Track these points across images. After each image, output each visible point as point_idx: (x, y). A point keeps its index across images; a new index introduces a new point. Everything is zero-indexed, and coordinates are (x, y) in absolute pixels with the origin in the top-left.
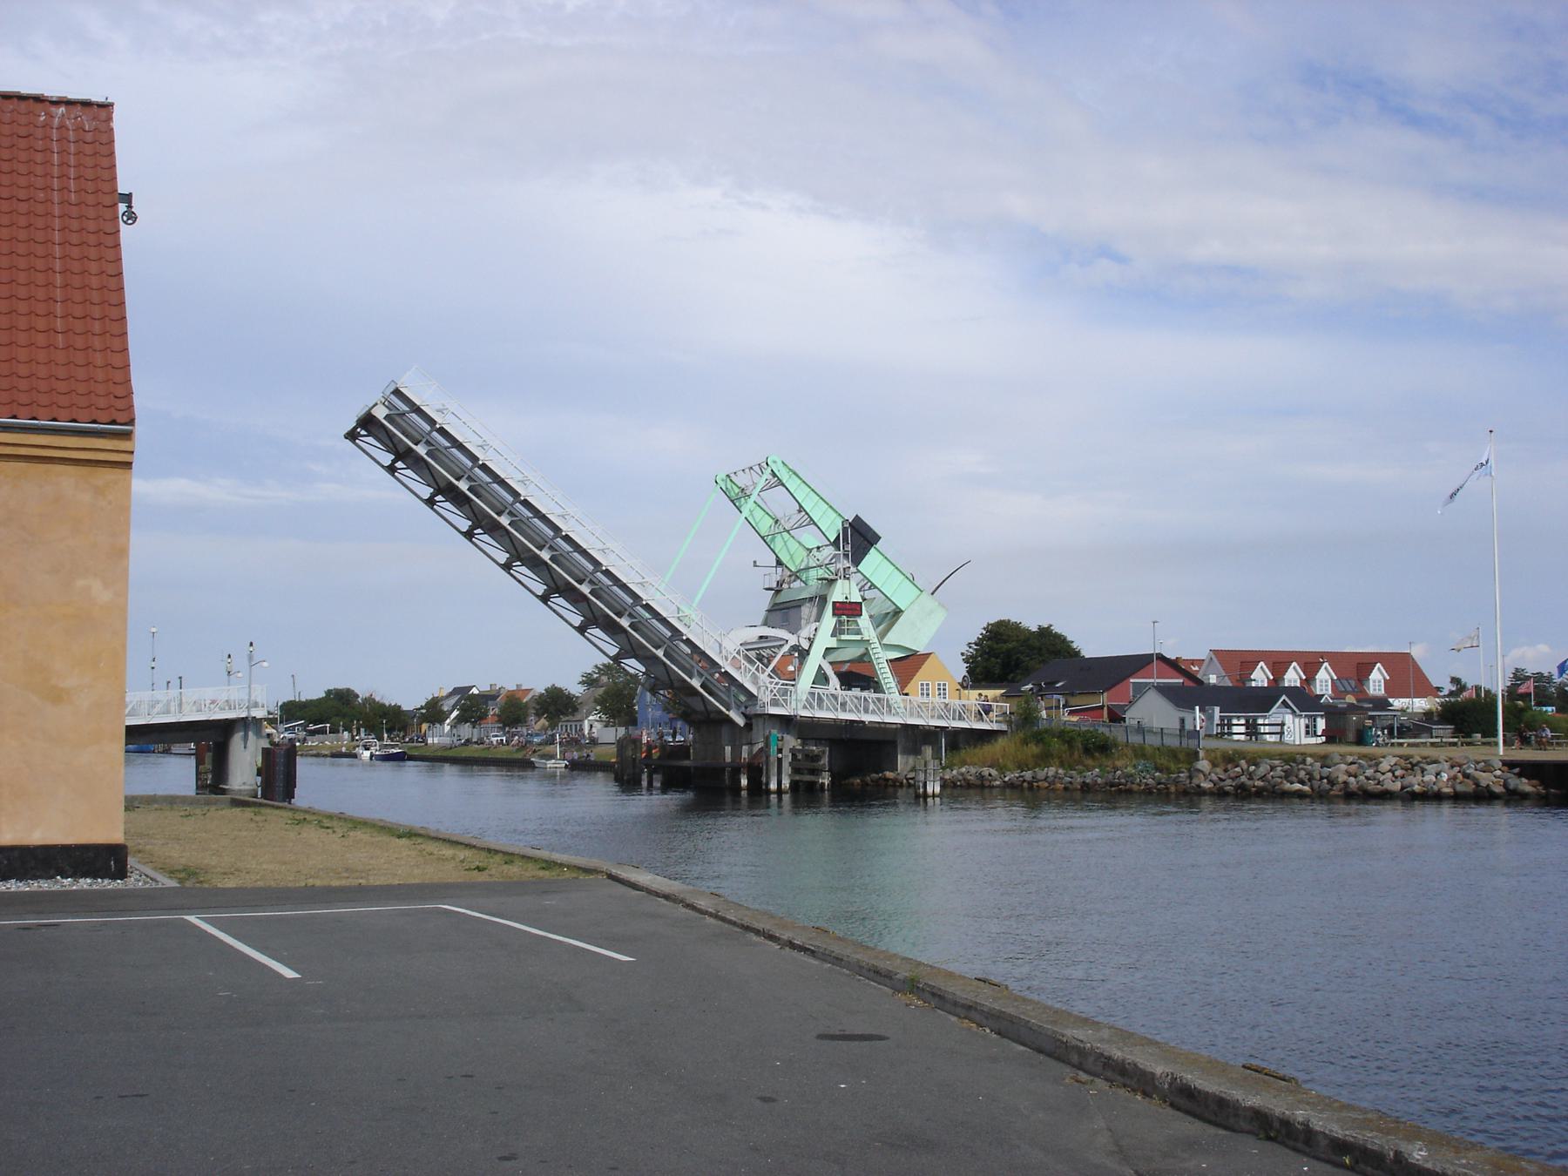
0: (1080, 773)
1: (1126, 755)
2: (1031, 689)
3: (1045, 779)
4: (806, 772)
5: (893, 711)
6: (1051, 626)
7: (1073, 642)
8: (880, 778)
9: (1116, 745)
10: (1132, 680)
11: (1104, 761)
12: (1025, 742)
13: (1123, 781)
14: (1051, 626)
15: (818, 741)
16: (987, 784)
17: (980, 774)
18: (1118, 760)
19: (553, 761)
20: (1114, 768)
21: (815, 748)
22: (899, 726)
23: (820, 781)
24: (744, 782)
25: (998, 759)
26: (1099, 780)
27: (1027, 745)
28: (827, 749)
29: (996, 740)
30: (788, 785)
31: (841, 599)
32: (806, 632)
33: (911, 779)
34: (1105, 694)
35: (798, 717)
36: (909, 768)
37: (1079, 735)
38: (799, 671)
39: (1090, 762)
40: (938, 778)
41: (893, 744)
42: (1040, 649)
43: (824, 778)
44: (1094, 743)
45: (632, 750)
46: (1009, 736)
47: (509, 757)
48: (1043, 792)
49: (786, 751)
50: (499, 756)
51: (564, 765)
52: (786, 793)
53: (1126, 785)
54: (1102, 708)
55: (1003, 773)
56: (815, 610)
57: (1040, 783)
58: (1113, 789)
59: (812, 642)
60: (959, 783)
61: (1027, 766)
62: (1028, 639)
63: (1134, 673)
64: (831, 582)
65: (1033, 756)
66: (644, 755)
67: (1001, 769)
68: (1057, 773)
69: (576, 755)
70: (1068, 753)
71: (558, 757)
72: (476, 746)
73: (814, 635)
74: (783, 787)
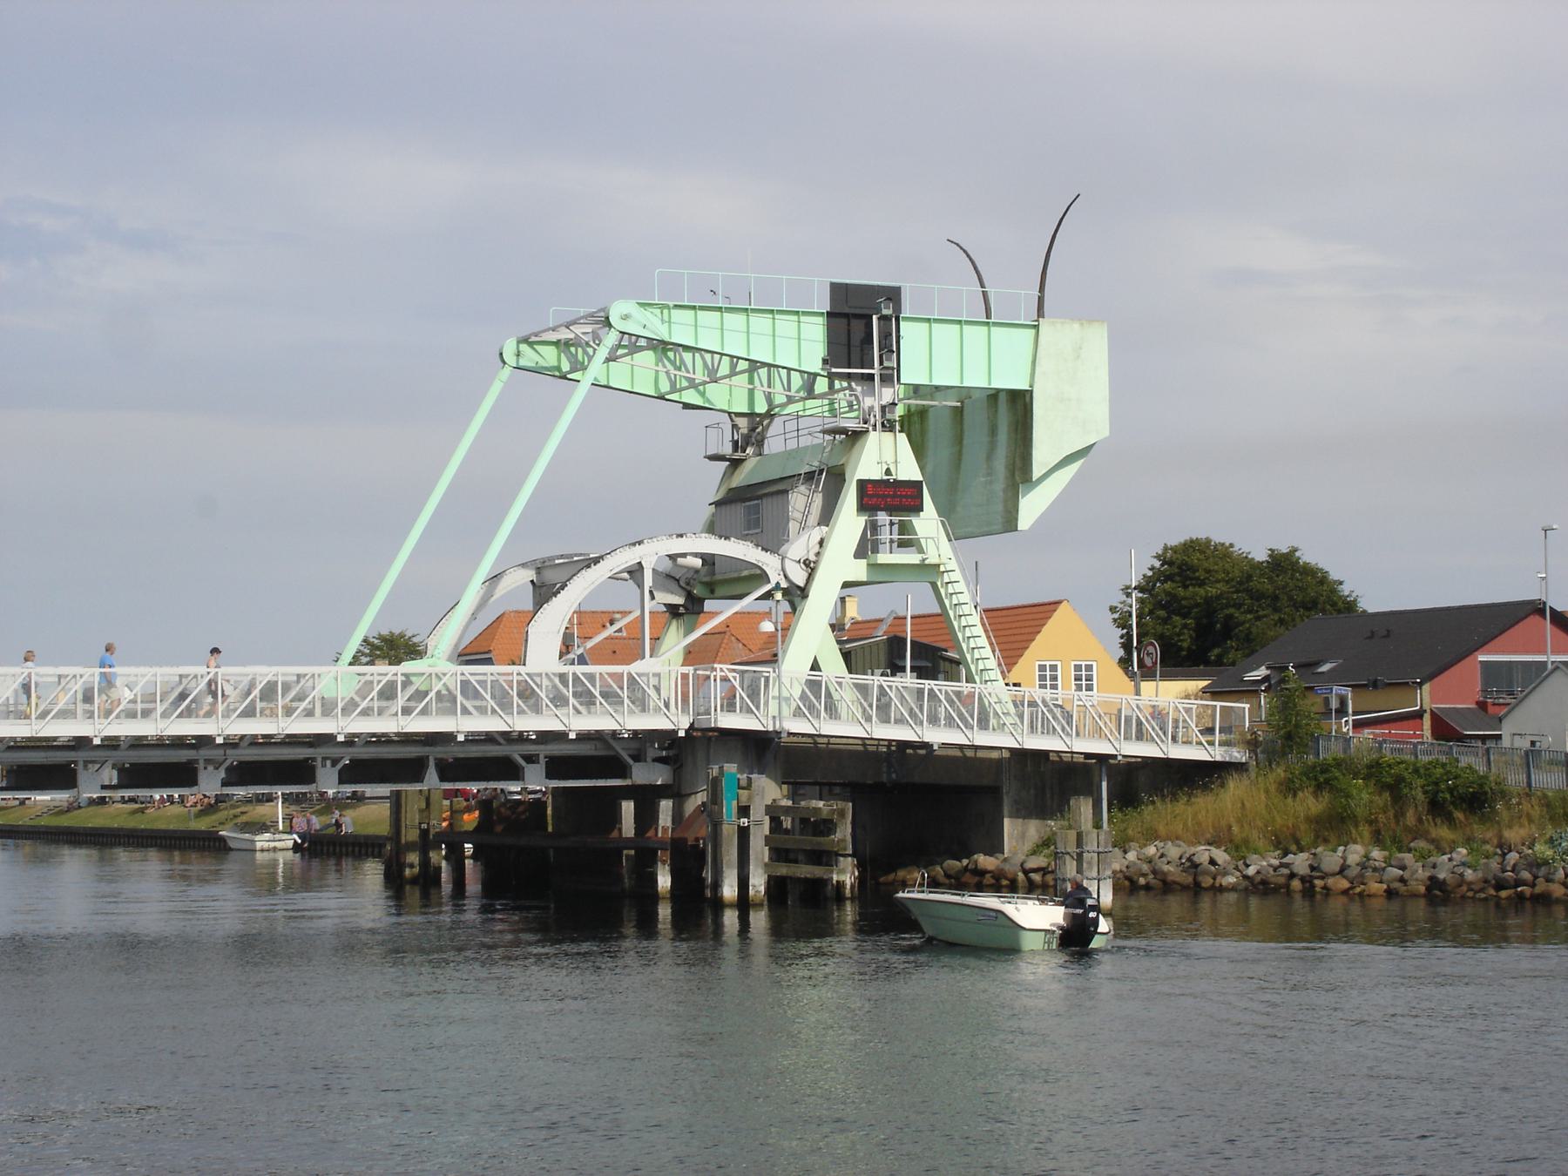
0: (1422, 857)
1: (1529, 817)
2: (1266, 679)
3: (1342, 871)
4: (801, 857)
5: (993, 722)
6: (1296, 550)
7: (1341, 583)
8: (966, 869)
9: (1504, 795)
10: (1482, 658)
11: (1479, 831)
12: (1289, 788)
13: (1526, 875)
14: (1296, 550)
15: (826, 789)
16: (1207, 881)
17: (1189, 859)
18: (1510, 827)
19: (267, 836)
20: (1500, 846)
21: (821, 804)
22: (1006, 754)
23: (835, 878)
24: (664, 881)
25: (1230, 827)
26: (1469, 874)
27: (1295, 795)
28: (851, 804)
29: (1222, 785)
30: (762, 889)
31: (876, 474)
32: (800, 547)
33: (1035, 870)
34: (1426, 687)
35: (784, 735)
36: (1028, 846)
37: (1416, 771)
38: (784, 636)
39: (1443, 832)
40: (1109, 873)
41: (994, 792)
42: (1276, 598)
43: (842, 871)
44: (1451, 790)
45: (421, 811)
46: (1253, 775)
47: (182, 827)
48: (1336, 905)
49: (758, 813)
50: (163, 827)
51: (290, 844)
52: (759, 905)
53: (1533, 885)
54: (1419, 715)
55: (1244, 858)
56: (818, 500)
57: (1330, 881)
58: (1504, 894)
59: (812, 569)
60: (1142, 881)
61: (1297, 842)
62: (1249, 578)
63: (1481, 646)
64: (855, 437)
65: (1308, 820)
66: (444, 824)
67: (1237, 848)
68: (1367, 857)
69: (317, 823)
70: (1391, 813)
71: (281, 828)
72: (120, 805)
73: (818, 554)
74: (751, 892)
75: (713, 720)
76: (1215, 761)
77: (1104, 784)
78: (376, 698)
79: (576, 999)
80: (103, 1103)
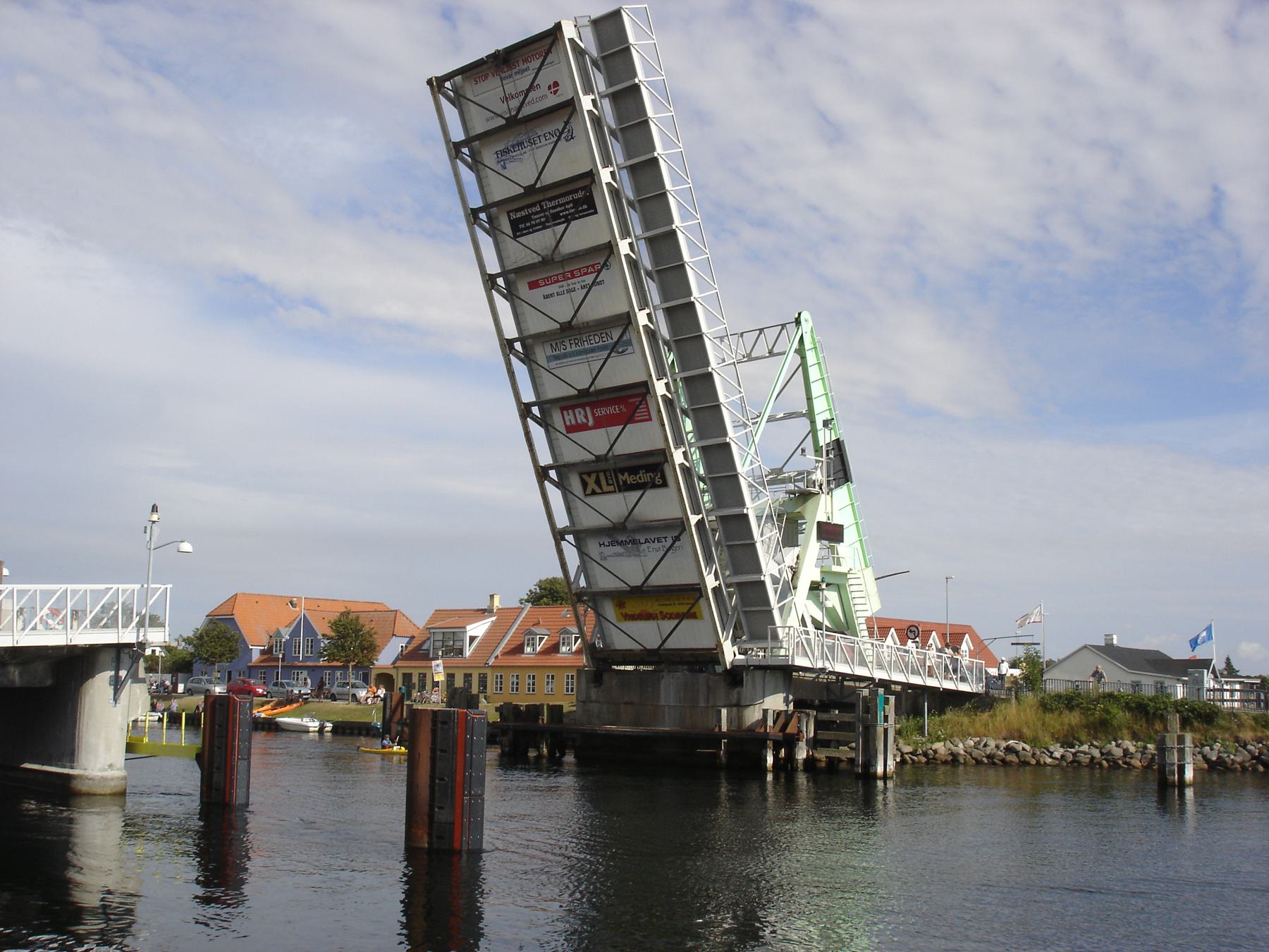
31: (825, 520)
73: (797, 563)
75: (790, 660)
76: (925, 686)
77: (926, 704)
78: (89, 626)
79: (537, 850)
80: (209, 935)
